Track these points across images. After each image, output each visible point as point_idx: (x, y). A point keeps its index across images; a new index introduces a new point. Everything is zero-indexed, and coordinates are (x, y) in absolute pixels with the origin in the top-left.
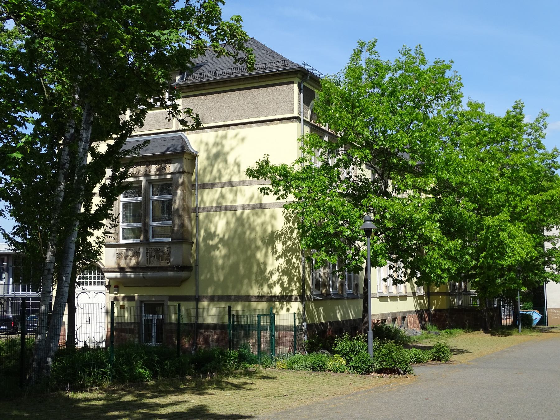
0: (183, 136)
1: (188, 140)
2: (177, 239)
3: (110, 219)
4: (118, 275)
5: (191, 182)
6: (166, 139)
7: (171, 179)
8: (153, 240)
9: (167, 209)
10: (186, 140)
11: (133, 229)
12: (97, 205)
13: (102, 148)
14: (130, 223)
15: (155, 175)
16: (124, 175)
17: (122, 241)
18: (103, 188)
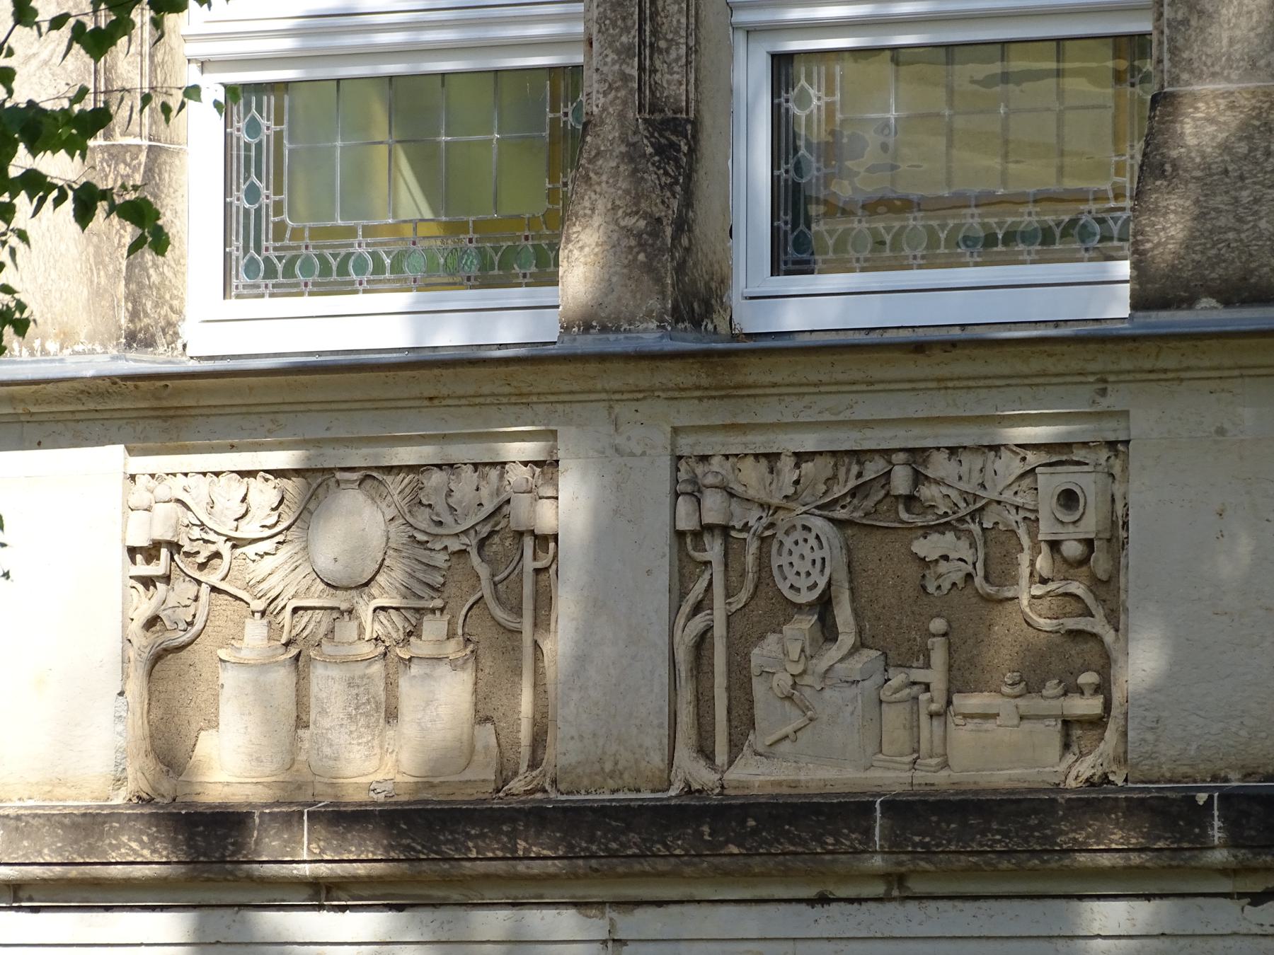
2: (1231, 295)
8: (816, 305)
17: (221, 322)
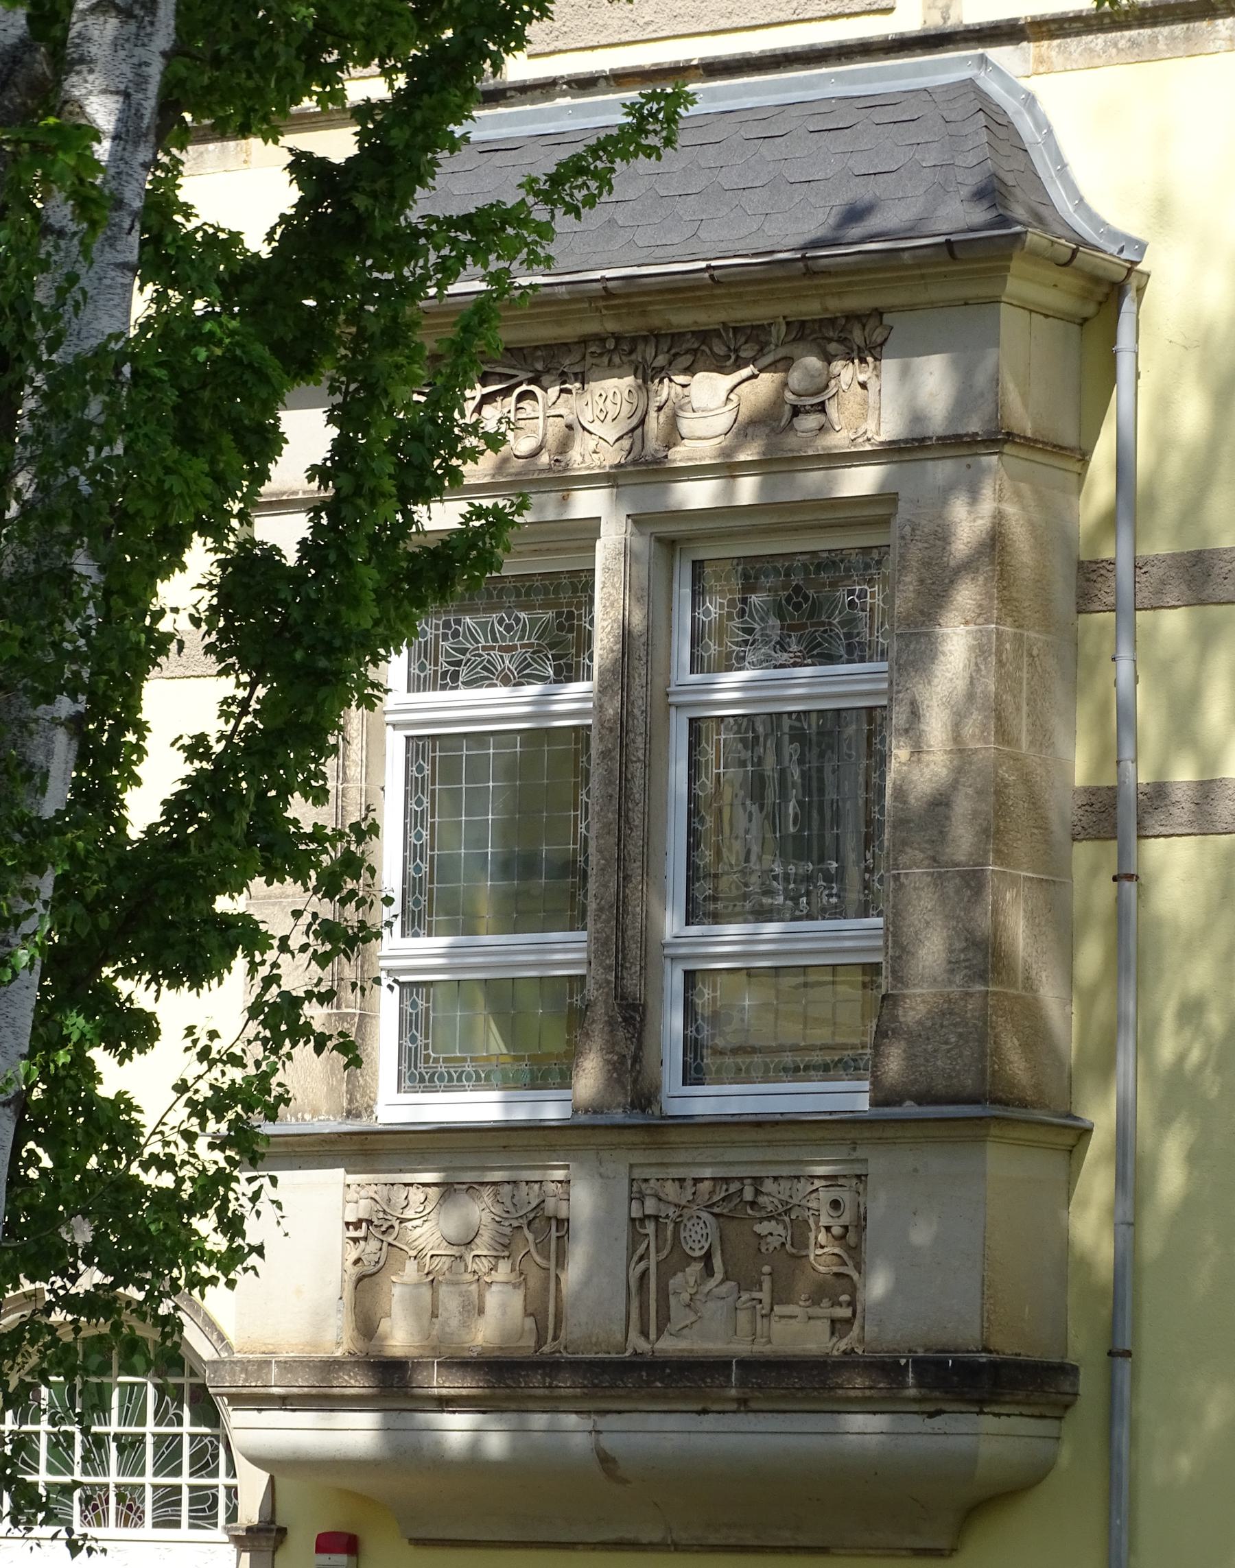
0: (993, 87)
1: (1043, 125)
2: (921, 1100)
3: (300, 876)
4: (356, 1432)
5: (1067, 539)
6: (830, 121)
7: (884, 500)
8: (706, 1102)
9: (815, 805)
10: (1025, 126)
11: (502, 996)
12: (197, 748)
13: (240, 190)
14: (470, 931)
15: (727, 469)
16: (425, 460)
17: (395, 1107)
18: (248, 574)
